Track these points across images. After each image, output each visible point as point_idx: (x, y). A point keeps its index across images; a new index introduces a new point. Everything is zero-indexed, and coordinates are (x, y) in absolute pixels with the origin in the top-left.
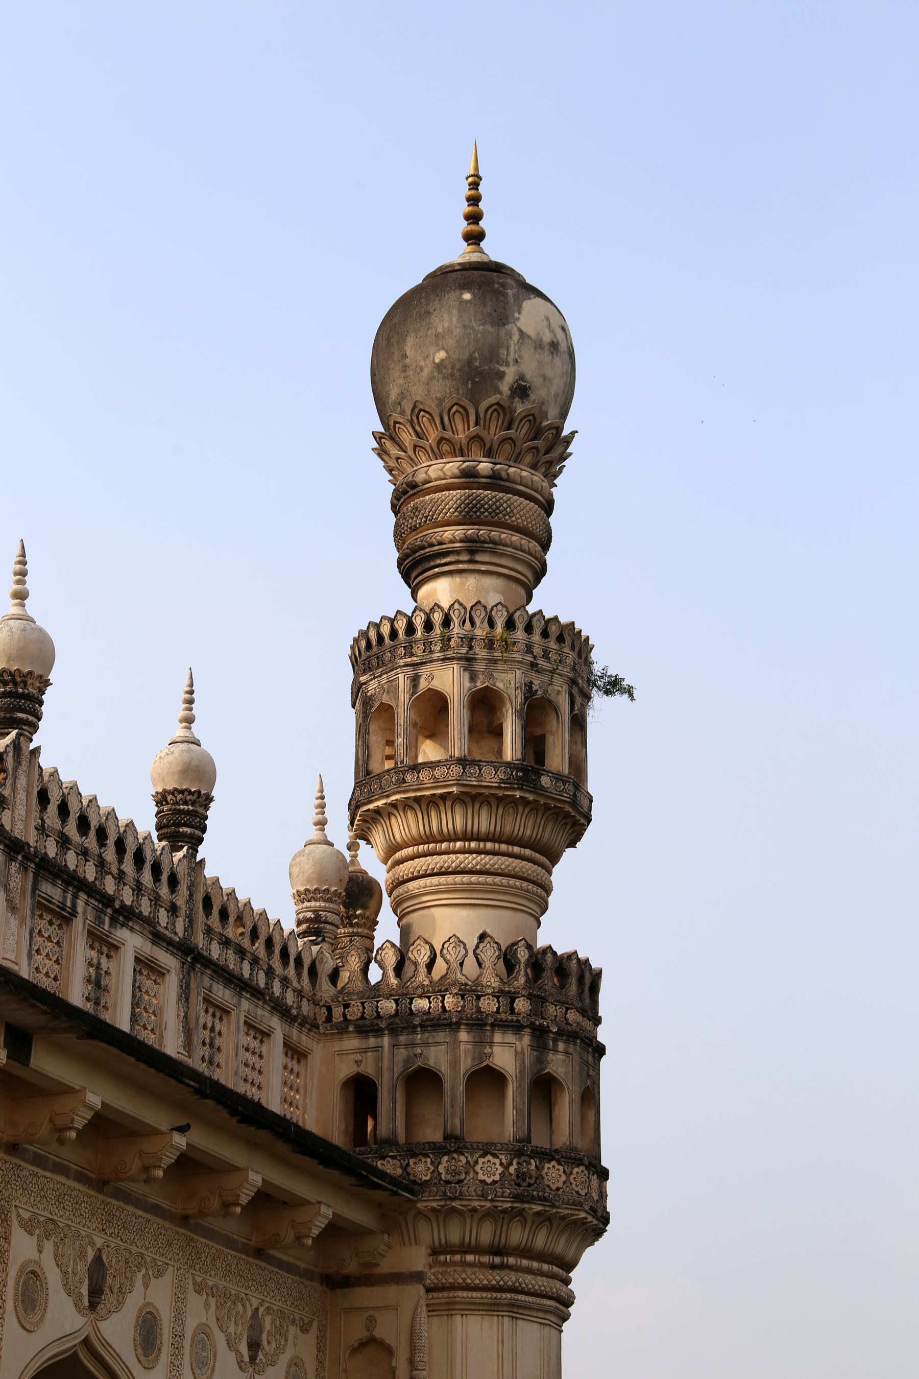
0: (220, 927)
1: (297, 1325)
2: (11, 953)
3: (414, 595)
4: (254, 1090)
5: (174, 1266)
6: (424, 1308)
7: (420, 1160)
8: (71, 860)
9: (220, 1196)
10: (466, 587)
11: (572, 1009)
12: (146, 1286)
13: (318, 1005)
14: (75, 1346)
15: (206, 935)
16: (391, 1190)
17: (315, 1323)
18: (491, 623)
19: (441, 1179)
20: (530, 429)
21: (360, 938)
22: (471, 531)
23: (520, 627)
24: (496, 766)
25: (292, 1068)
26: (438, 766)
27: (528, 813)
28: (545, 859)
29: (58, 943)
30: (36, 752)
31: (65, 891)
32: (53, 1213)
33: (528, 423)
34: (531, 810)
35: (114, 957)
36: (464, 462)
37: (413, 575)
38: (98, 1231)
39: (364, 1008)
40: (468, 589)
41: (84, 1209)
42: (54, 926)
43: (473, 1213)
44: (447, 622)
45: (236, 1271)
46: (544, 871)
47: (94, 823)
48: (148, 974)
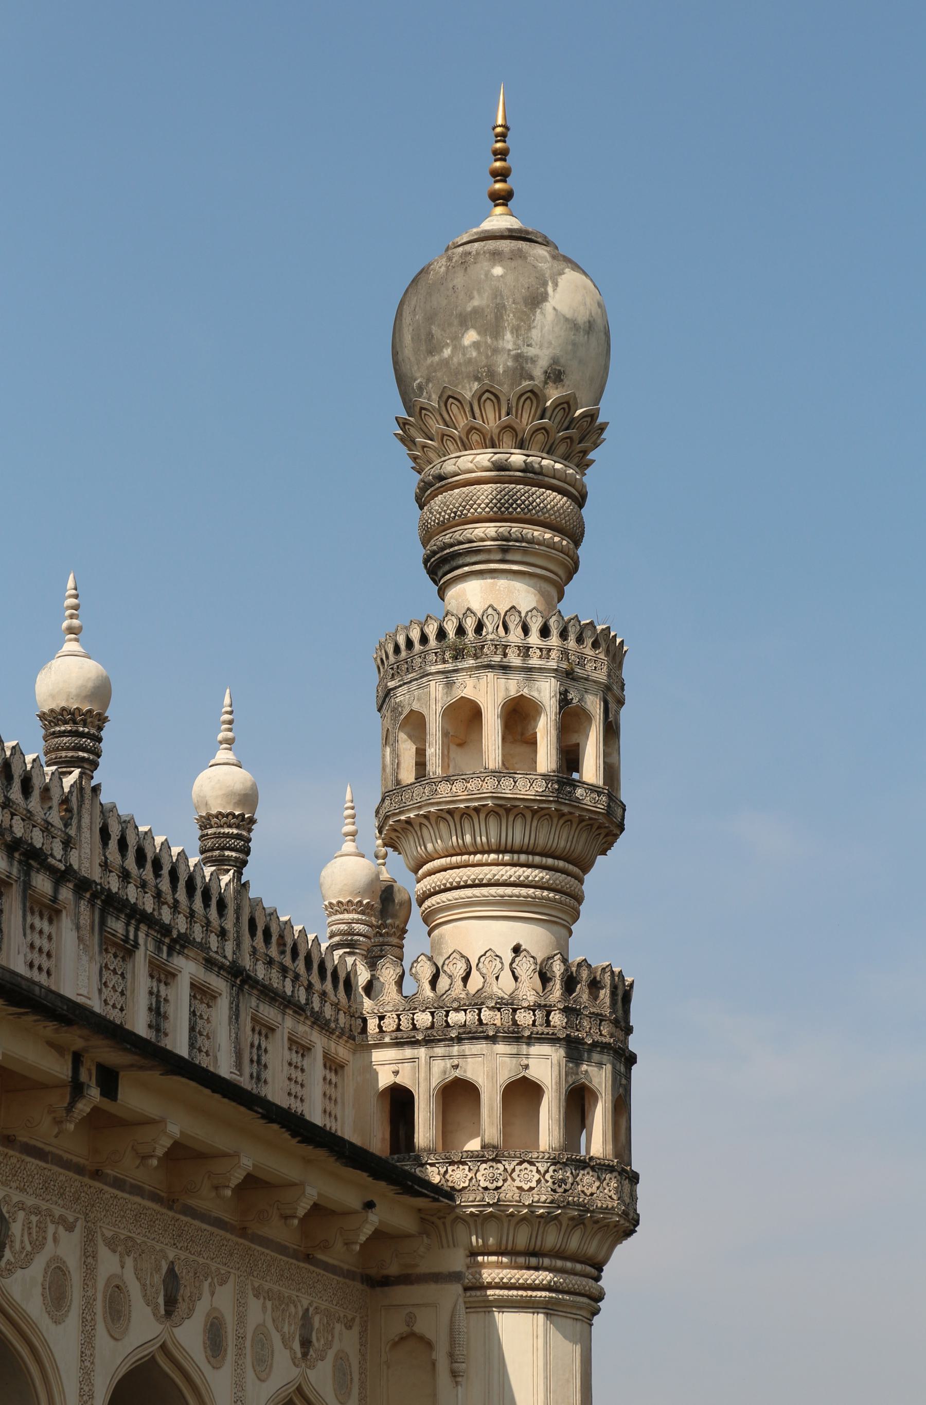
0: (264, 947)
1: (341, 1322)
2: (83, 988)
3: (441, 593)
4: (299, 1103)
5: (235, 1274)
6: (463, 1306)
8: (132, 893)
9: (278, 1209)
10: (498, 587)
11: (606, 1020)
12: (213, 1294)
13: (354, 1016)
14: (290, 1393)
15: (252, 956)
16: (433, 1197)
17: (358, 1320)
18: (526, 630)
19: (479, 1185)
21: (390, 947)
22: (503, 528)
23: (555, 632)
24: (531, 778)
25: (331, 1080)
26: (472, 778)
27: (562, 825)
28: (580, 871)
29: (122, 974)
30: (96, 790)
31: (128, 924)
32: (132, 1232)
33: (562, 410)
35: (213, 1006)
36: (496, 453)
37: (440, 573)
38: (170, 1245)
39: (400, 1020)
40: (499, 590)
41: (157, 1226)
42: (119, 959)
43: (510, 1218)
44: (479, 627)
45: (288, 1276)
46: (577, 881)
47: (150, 856)
48: (201, 998)
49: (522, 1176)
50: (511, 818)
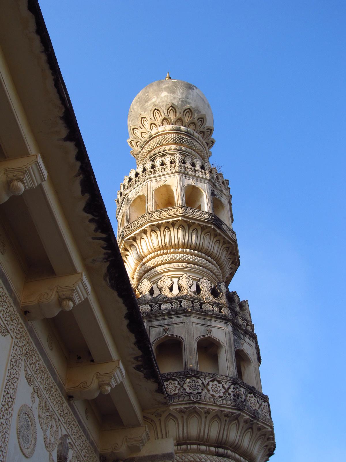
7: (171, 383)
9: (57, 292)
11: (249, 326)
20: (201, 125)
33: (201, 121)
34: (217, 240)
43: (207, 414)
49: (214, 389)
50: (191, 231)
